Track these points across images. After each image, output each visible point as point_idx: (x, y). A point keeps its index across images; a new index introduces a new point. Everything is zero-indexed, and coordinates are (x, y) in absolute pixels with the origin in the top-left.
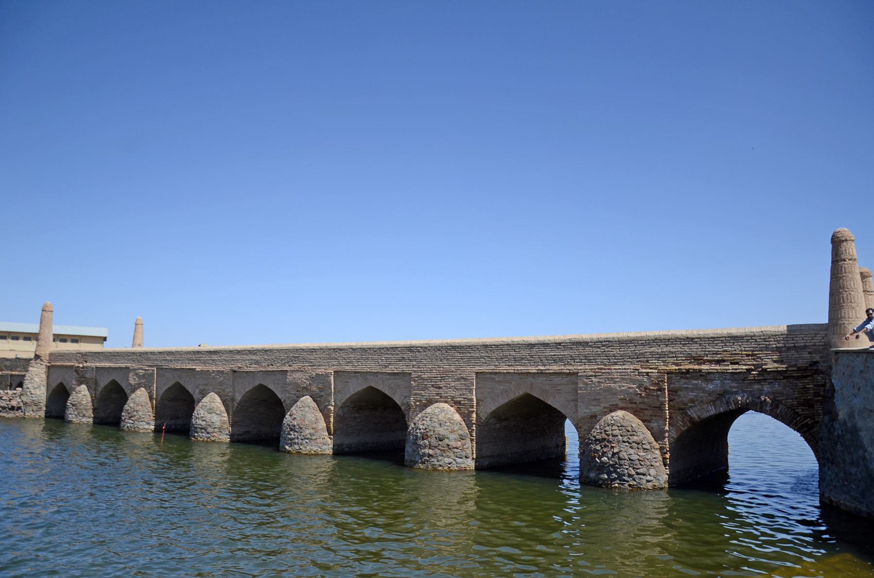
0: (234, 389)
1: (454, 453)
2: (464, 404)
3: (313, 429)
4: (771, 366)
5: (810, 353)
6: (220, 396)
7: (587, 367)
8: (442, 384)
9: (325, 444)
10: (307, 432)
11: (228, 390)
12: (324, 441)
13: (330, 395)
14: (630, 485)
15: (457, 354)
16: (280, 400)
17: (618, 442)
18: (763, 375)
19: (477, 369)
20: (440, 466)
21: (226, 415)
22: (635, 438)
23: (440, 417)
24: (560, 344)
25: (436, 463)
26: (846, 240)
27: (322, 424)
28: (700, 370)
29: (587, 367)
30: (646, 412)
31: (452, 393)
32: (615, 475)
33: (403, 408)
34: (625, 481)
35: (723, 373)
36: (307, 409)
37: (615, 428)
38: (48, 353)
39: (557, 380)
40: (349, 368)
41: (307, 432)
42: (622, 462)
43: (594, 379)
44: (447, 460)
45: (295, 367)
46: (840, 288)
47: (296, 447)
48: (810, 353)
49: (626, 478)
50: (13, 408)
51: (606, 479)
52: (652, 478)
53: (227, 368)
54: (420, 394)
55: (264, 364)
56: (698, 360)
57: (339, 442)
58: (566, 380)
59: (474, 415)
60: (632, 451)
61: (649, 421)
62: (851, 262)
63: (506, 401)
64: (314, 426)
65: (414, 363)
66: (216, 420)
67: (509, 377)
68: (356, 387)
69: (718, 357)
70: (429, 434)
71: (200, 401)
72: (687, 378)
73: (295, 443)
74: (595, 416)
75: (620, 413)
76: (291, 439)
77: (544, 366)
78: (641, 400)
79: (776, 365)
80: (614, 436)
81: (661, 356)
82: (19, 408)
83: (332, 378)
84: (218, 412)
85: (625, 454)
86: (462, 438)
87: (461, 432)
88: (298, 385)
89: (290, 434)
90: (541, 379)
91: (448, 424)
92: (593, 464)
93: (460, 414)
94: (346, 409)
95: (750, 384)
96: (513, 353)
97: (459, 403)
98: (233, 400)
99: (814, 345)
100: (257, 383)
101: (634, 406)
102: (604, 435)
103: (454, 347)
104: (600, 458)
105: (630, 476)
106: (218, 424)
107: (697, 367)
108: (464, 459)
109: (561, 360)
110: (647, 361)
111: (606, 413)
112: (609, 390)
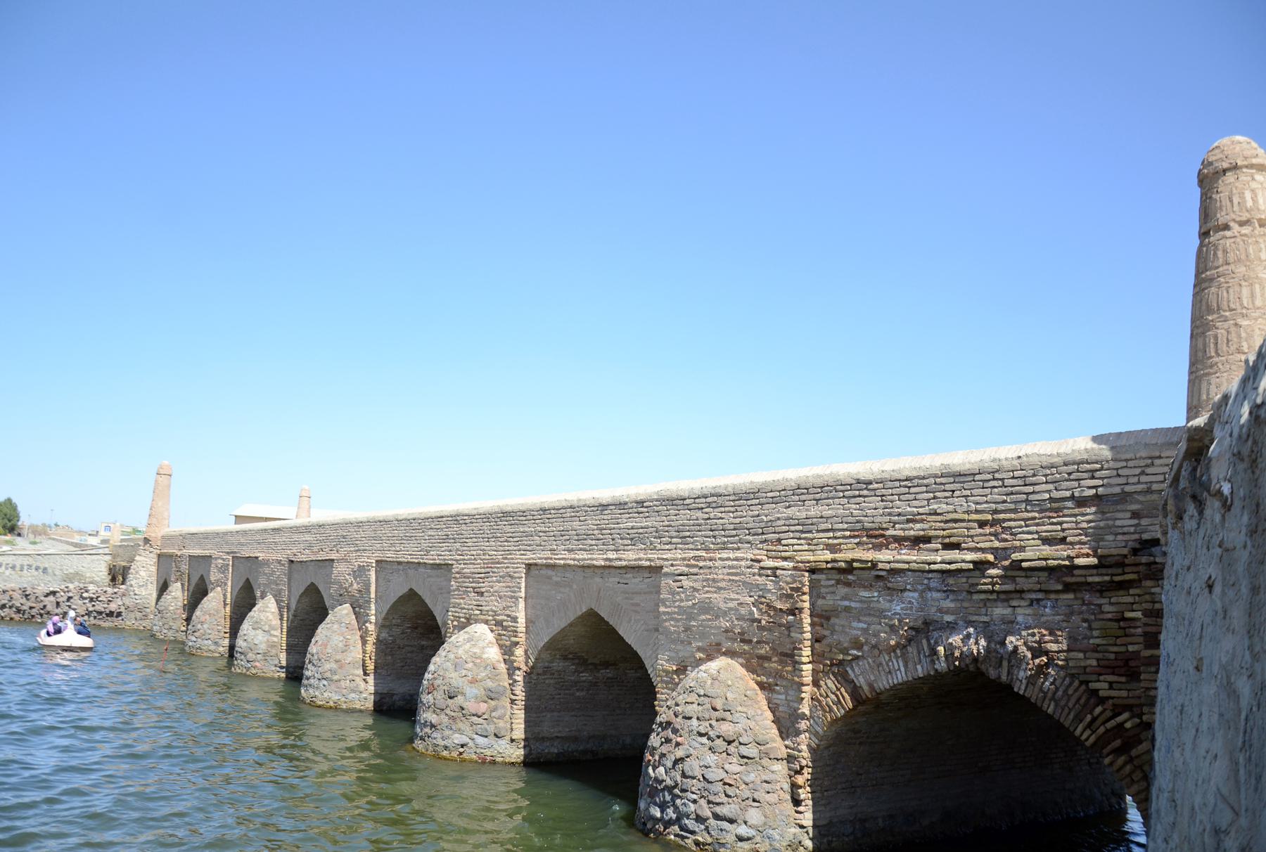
3: (337, 661)
4: (1034, 552)
5: (1135, 515)
7: (679, 554)
8: (484, 587)
9: (353, 691)
10: (327, 666)
13: (369, 602)
14: (697, 843)
15: (508, 529)
18: (1013, 578)
19: (531, 557)
20: (446, 748)
21: (277, 633)
22: (726, 729)
24: (641, 503)
26: (1235, 167)
28: (874, 565)
35: (923, 573)
38: (160, 535)
43: (686, 582)
44: (458, 739)
46: (1210, 311)
48: (1135, 515)
49: (690, 823)
50: (111, 614)
51: (657, 820)
52: (751, 832)
56: (877, 537)
60: (711, 759)
62: (1246, 230)
68: (398, 589)
69: (916, 530)
72: (848, 584)
79: (1047, 550)
81: (805, 527)
82: (119, 614)
83: (373, 575)
84: (266, 628)
86: (491, 696)
87: (490, 684)
91: (470, 665)
93: (501, 646)
94: (396, 631)
95: (985, 601)
96: (576, 524)
99: (1149, 491)
103: (505, 515)
104: (655, 768)
105: (700, 819)
107: (870, 555)
108: (492, 740)
112: (706, 607)
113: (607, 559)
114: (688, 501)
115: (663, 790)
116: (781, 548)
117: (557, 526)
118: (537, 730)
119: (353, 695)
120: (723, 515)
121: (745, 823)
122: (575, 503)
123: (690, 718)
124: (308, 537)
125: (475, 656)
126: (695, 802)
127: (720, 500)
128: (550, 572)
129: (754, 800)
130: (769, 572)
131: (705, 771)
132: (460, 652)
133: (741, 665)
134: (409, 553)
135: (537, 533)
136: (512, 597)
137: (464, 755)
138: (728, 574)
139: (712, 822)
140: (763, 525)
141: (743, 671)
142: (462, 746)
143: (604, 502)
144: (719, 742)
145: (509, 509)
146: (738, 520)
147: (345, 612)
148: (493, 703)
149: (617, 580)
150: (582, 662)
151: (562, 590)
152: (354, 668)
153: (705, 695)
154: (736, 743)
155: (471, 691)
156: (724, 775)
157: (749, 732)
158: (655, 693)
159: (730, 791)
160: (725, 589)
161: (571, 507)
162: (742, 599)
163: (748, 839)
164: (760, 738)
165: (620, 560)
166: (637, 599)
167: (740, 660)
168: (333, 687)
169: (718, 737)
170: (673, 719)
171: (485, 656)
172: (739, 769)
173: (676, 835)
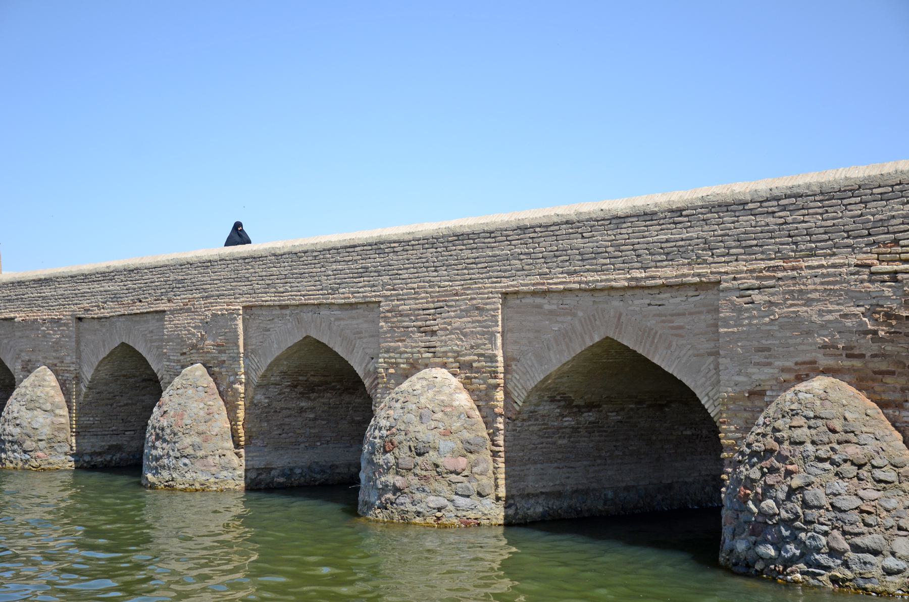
0: (79, 357)
1: (450, 483)
2: (478, 370)
3: (199, 434)
6: (56, 373)
7: (742, 266)
8: (437, 324)
9: (224, 468)
10: (187, 441)
11: (68, 360)
12: (223, 460)
13: (236, 359)
14: (834, 580)
15: (467, 253)
16: (155, 375)
17: (805, 458)
19: (507, 284)
20: (418, 514)
21: (65, 412)
22: (851, 451)
23: (423, 400)
24: (679, 211)
25: (410, 507)
27: (222, 423)
29: (742, 266)
30: (889, 380)
31: (457, 344)
32: (792, 549)
33: (367, 382)
34: (819, 566)
36: (190, 391)
37: (799, 421)
39: (673, 302)
40: (268, 298)
41: (187, 441)
42: (813, 514)
43: (757, 297)
44: (434, 501)
45: (178, 303)
47: (165, 474)
49: (822, 559)
51: (772, 560)
52: (902, 565)
53: (65, 314)
54: (395, 350)
55: (126, 300)
57: (259, 463)
58: (694, 300)
59: (500, 395)
60: (840, 486)
61: (899, 406)
63: (567, 357)
64: (202, 428)
65: (386, 279)
66: (41, 421)
67: (570, 301)
68: (283, 338)
70: (396, 439)
71: (21, 381)
73: (163, 467)
74: (762, 393)
75: (818, 384)
76: (157, 459)
77: (645, 269)
78: (875, 348)
80: (794, 443)
83: (240, 323)
84: (48, 406)
85: (820, 492)
86: (470, 449)
87: (466, 435)
88: (181, 341)
89: (155, 448)
90: (640, 302)
91: (439, 415)
92: (743, 517)
93: (471, 392)
94: (274, 391)
96: (578, 242)
97: (469, 366)
98: (78, 379)
100: (117, 343)
101: (857, 363)
102: (771, 443)
103: (460, 237)
104: (757, 501)
105: (833, 553)
106: (46, 432)
108: (475, 500)
109: (682, 253)
110: (896, 242)
111: (784, 386)
112: (795, 322)
113: (632, 279)
114: (751, 206)
115: (777, 524)
116: (899, 249)
117: (546, 245)
118: (522, 485)
119: (225, 473)
120: (807, 218)
121: (893, 554)
122: (574, 218)
123: (802, 443)
124: (107, 286)
125: (443, 404)
126: (826, 534)
127: (800, 202)
128: (538, 300)
129: (900, 528)
130: (886, 277)
131: (834, 500)
132: (423, 400)
133: (850, 384)
134: (303, 291)
135: (517, 256)
136: (483, 333)
137: (444, 520)
138: (822, 283)
139: (851, 555)
140: (870, 225)
141: (852, 390)
142: (439, 510)
143: (620, 214)
144: (847, 467)
145: (467, 230)
146: (830, 223)
147: (198, 373)
148: (472, 457)
149: (648, 301)
150: (568, 404)
151: (559, 319)
152: (223, 439)
153: (816, 417)
154: (868, 467)
155: (445, 445)
156: (858, 502)
157: (882, 454)
158: (717, 428)
159: (870, 519)
160: (818, 300)
161: (567, 222)
162: (846, 310)
163: (899, 572)
164: (897, 460)
165: (653, 278)
166: (679, 322)
167: (847, 378)
168: (198, 464)
169: (845, 461)
170: (776, 446)
171: (456, 404)
172: (876, 495)
173: (802, 573)
